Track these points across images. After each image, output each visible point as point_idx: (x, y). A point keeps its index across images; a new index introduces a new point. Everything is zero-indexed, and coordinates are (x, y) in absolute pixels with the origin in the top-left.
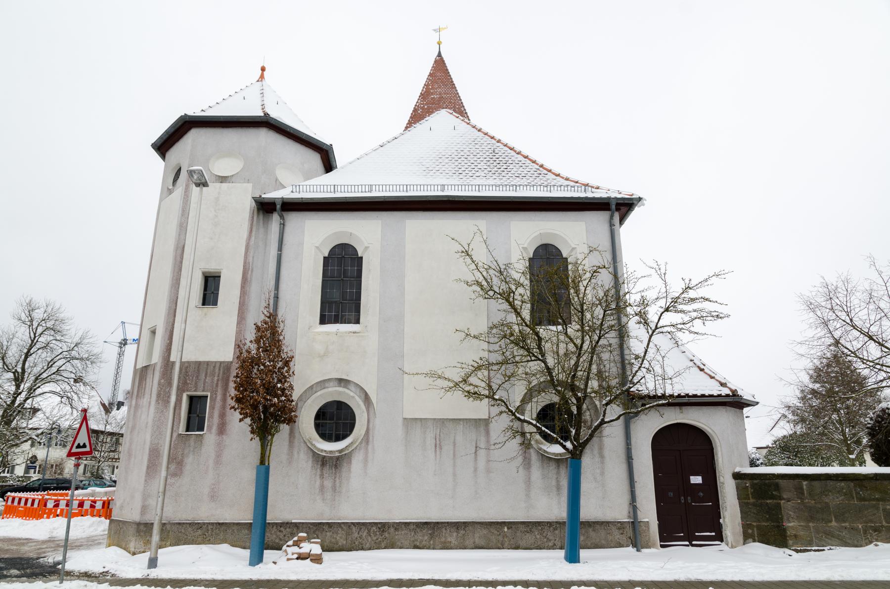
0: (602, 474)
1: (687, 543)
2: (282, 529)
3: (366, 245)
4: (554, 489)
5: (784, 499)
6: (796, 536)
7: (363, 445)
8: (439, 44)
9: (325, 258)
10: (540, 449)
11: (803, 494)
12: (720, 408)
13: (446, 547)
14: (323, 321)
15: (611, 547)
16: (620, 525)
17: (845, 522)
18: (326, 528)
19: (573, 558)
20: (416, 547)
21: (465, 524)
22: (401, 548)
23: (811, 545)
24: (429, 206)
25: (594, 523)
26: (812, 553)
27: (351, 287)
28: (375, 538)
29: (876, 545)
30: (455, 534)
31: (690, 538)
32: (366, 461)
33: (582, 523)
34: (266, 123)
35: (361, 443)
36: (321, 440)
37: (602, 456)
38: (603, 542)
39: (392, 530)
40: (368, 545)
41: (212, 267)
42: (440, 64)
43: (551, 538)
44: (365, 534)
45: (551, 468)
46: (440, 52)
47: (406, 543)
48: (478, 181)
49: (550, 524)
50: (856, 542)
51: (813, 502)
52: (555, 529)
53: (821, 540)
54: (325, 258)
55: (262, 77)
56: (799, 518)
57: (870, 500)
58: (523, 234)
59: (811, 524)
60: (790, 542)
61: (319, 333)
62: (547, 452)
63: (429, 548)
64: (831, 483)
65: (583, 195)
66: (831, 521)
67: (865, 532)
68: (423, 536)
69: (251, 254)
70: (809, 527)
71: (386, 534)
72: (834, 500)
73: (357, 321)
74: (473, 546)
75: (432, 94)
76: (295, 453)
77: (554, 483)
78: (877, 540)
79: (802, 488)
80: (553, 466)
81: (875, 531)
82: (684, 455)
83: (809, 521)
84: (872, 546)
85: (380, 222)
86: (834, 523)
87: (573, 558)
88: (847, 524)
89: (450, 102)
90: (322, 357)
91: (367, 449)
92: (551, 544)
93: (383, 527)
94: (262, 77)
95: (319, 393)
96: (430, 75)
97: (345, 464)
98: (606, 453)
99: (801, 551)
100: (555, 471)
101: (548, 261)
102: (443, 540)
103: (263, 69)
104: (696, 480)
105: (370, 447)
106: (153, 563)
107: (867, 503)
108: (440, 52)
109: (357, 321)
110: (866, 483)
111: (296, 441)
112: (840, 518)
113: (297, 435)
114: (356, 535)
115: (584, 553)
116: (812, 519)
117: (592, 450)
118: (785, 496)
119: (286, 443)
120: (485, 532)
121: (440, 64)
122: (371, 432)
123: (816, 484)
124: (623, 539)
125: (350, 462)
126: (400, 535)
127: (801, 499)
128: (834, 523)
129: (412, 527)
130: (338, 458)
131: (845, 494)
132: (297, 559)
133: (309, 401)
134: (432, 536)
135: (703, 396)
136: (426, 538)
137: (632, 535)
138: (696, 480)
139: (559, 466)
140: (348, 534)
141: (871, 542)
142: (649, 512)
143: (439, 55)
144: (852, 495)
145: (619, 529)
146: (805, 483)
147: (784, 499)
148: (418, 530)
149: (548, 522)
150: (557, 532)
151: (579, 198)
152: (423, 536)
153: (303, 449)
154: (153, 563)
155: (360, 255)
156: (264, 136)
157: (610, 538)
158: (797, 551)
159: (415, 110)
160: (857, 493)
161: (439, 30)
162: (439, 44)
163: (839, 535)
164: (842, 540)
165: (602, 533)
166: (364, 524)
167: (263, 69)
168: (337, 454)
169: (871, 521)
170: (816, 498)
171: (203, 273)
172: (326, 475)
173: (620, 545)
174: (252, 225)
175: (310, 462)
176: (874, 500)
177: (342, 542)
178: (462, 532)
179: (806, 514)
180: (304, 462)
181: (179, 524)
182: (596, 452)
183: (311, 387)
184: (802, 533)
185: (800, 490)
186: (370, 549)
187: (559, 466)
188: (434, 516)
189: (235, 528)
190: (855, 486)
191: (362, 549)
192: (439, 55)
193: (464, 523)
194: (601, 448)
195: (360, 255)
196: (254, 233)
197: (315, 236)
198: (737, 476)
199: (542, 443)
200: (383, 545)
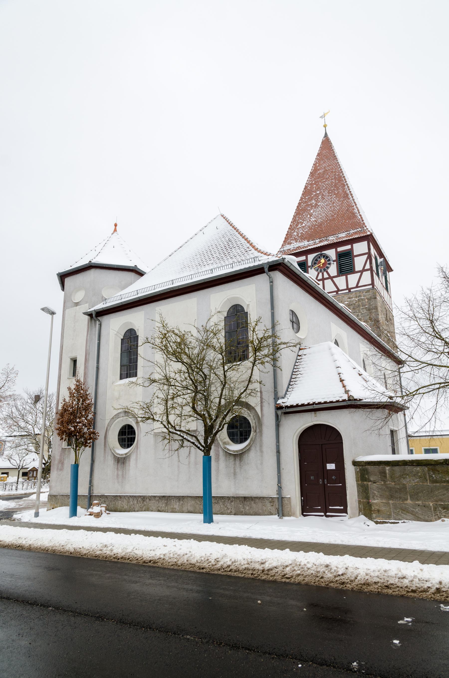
0: (262, 464)
1: (323, 514)
2: (101, 499)
3: (248, 303)
4: (232, 475)
5: (371, 481)
6: (379, 511)
7: (136, 450)
8: (325, 126)
9: (122, 339)
10: (225, 448)
11: (385, 477)
12: (345, 410)
13: (173, 511)
14: (121, 378)
15: (265, 515)
16: (271, 500)
17: (418, 500)
18: (119, 498)
19: (209, 520)
20: (159, 511)
21: (183, 497)
22: (152, 511)
23: (389, 518)
24: (129, 306)
25: (255, 498)
26: (389, 524)
27: (134, 356)
28: (140, 505)
29: (443, 521)
30: (178, 503)
31: (326, 511)
32: (136, 460)
33: (214, 497)
34: (90, 267)
35: (134, 449)
36: (120, 448)
37: (262, 452)
38: (260, 511)
39: (148, 500)
40: (137, 509)
41: (73, 355)
42: (326, 144)
43: (229, 507)
44: (136, 502)
45: (231, 461)
46: (326, 134)
47: (154, 508)
48: (207, 268)
49: (229, 498)
50: (426, 518)
51: (393, 483)
52: (232, 502)
53: (398, 514)
54: (122, 339)
55: (115, 230)
56: (382, 497)
57: (442, 482)
58: (218, 301)
59: (391, 502)
60: (374, 515)
61: (120, 385)
62: (228, 450)
63: (165, 512)
64: (408, 468)
65: (252, 265)
66: (407, 500)
67: (435, 509)
68: (162, 504)
69: (88, 345)
70: (388, 504)
71: (145, 503)
72: (410, 482)
73: (136, 376)
74: (187, 511)
75: (319, 170)
76: (106, 456)
77: (232, 471)
78: (445, 517)
79: (385, 473)
80: (232, 459)
81: (444, 508)
82: (320, 448)
83: (389, 499)
84: (439, 521)
85: (254, 285)
86: (409, 501)
87: (209, 520)
88: (420, 502)
89: (332, 172)
90: (118, 399)
91: (137, 452)
92: (229, 511)
93: (144, 498)
94: (115, 230)
95: (116, 421)
96: (318, 155)
97: (127, 462)
98: (264, 449)
99: (380, 523)
100: (233, 463)
101: (237, 316)
102: (172, 507)
103: (116, 225)
104: (331, 466)
105: (138, 451)
106: (37, 515)
107: (438, 484)
108: (326, 134)
109: (136, 376)
110: (439, 468)
111: (107, 449)
112: (415, 496)
113: (107, 446)
114: (132, 503)
115: (215, 517)
116: (391, 497)
117: (256, 447)
118: (372, 479)
119: (103, 451)
120: (193, 502)
121: (326, 144)
122: (139, 442)
123: (396, 468)
124: (273, 510)
125: (130, 461)
126: (152, 504)
127: (384, 481)
128: (409, 501)
129: (157, 498)
130: (124, 458)
131: (420, 477)
132: (89, 515)
133: (113, 426)
134: (167, 504)
135: (325, 403)
136: (164, 505)
137: (279, 507)
138: (331, 466)
139: (235, 459)
140: (128, 502)
141: (439, 518)
142: (293, 491)
143: (326, 134)
144: (425, 478)
145: (270, 502)
146: (387, 468)
147: (371, 481)
148: (160, 500)
149: (228, 497)
150: (233, 503)
151: (250, 267)
152: (162, 504)
153: (110, 453)
154: (37, 515)
155: (246, 311)
156: (93, 273)
157: (265, 508)
158: (377, 523)
159: (306, 188)
160: (430, 476)
161: (323, 117)
162: (325, 126)
163: (413, 511)
164: (415, 515)
165: (260, 505)
166: (135, 496)
167: (116, 225)
168: (124, 456)
169: (441, 500)
170: (396, 480)
171: (71, 359)
172: (119, 468)
173: (271, 514)
174: (88, 328)
175: (113, 461)
176: (444, 482)
177: (126, 507)
178: (182, 502)
179: (387, 493)
180: (110, 461)
181: (62, 495)
182: (258, 448)
183: (113, 418)
184: (383, 508)
185: (383, 473)
186: (138, 511)
187: (235, 459)
188: (168, 492)
189: (83, 498)
190: (429, 470)
191: (134, 511)
192: (326, 134)
193: (183, 496)
194: (261, 446)
195: (246, 311)
196: (89, 332)
197: (115, 326)
198: (355, 463)
199: (228, 444)
200: (144, 509)
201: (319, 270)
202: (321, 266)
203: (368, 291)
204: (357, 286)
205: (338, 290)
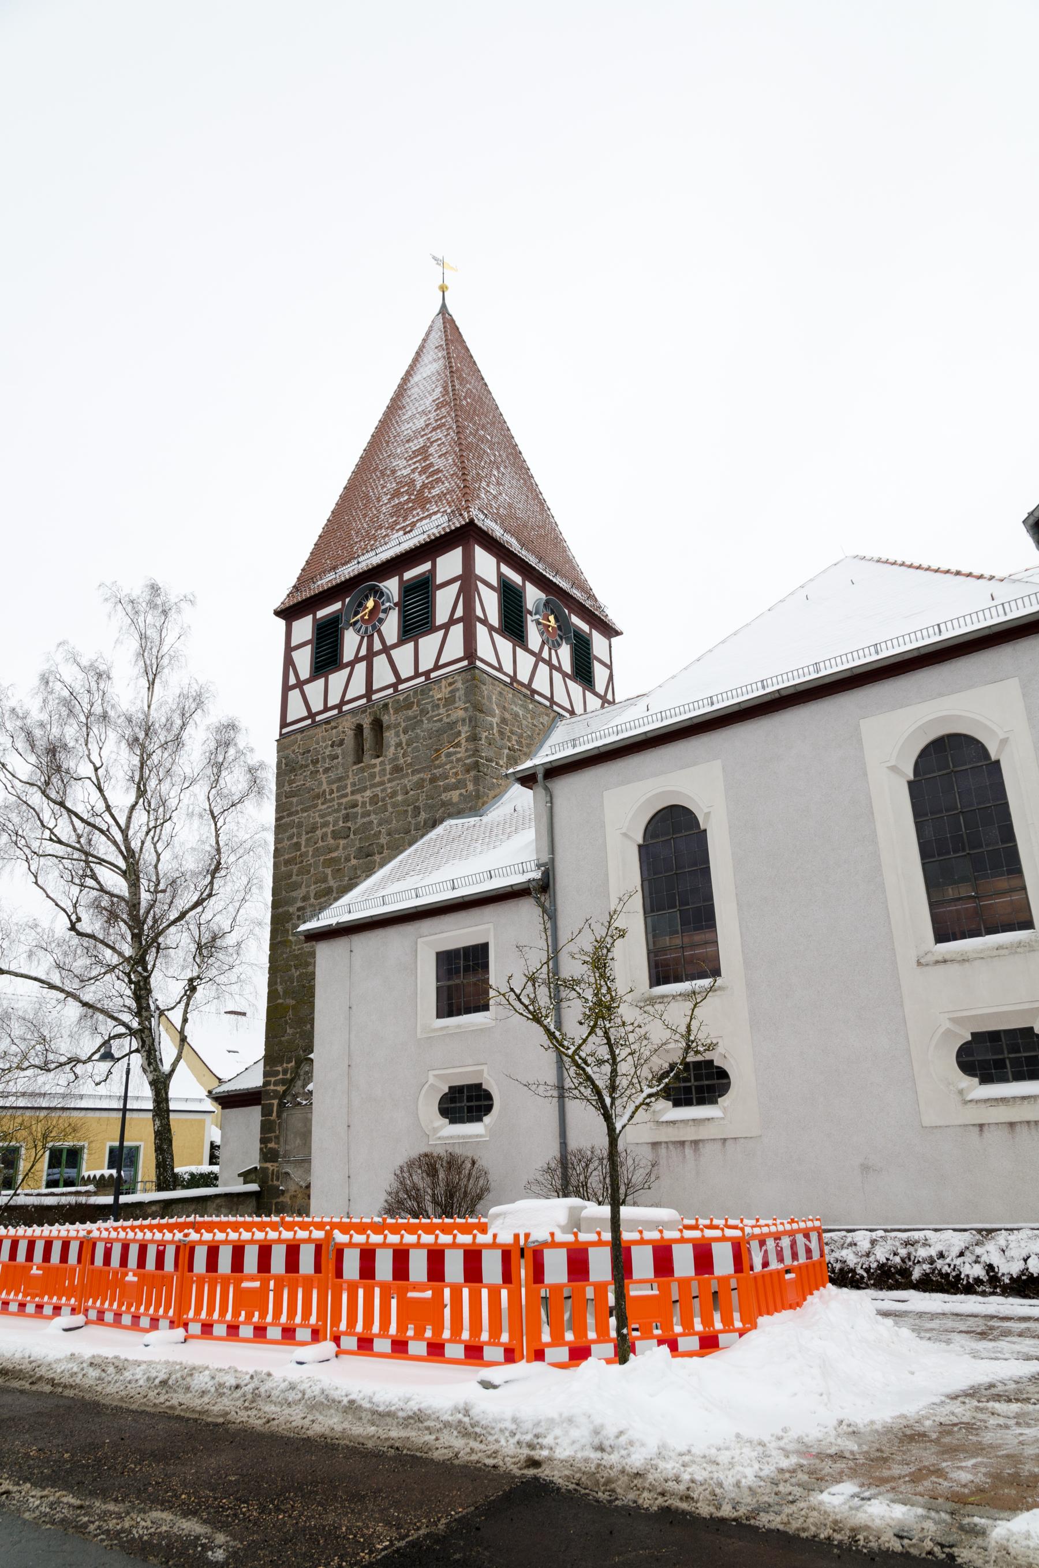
201: (363, 629)
202: (366, 617)
203: (464, 670)
204: (437, 667)
205: (400, 681)
